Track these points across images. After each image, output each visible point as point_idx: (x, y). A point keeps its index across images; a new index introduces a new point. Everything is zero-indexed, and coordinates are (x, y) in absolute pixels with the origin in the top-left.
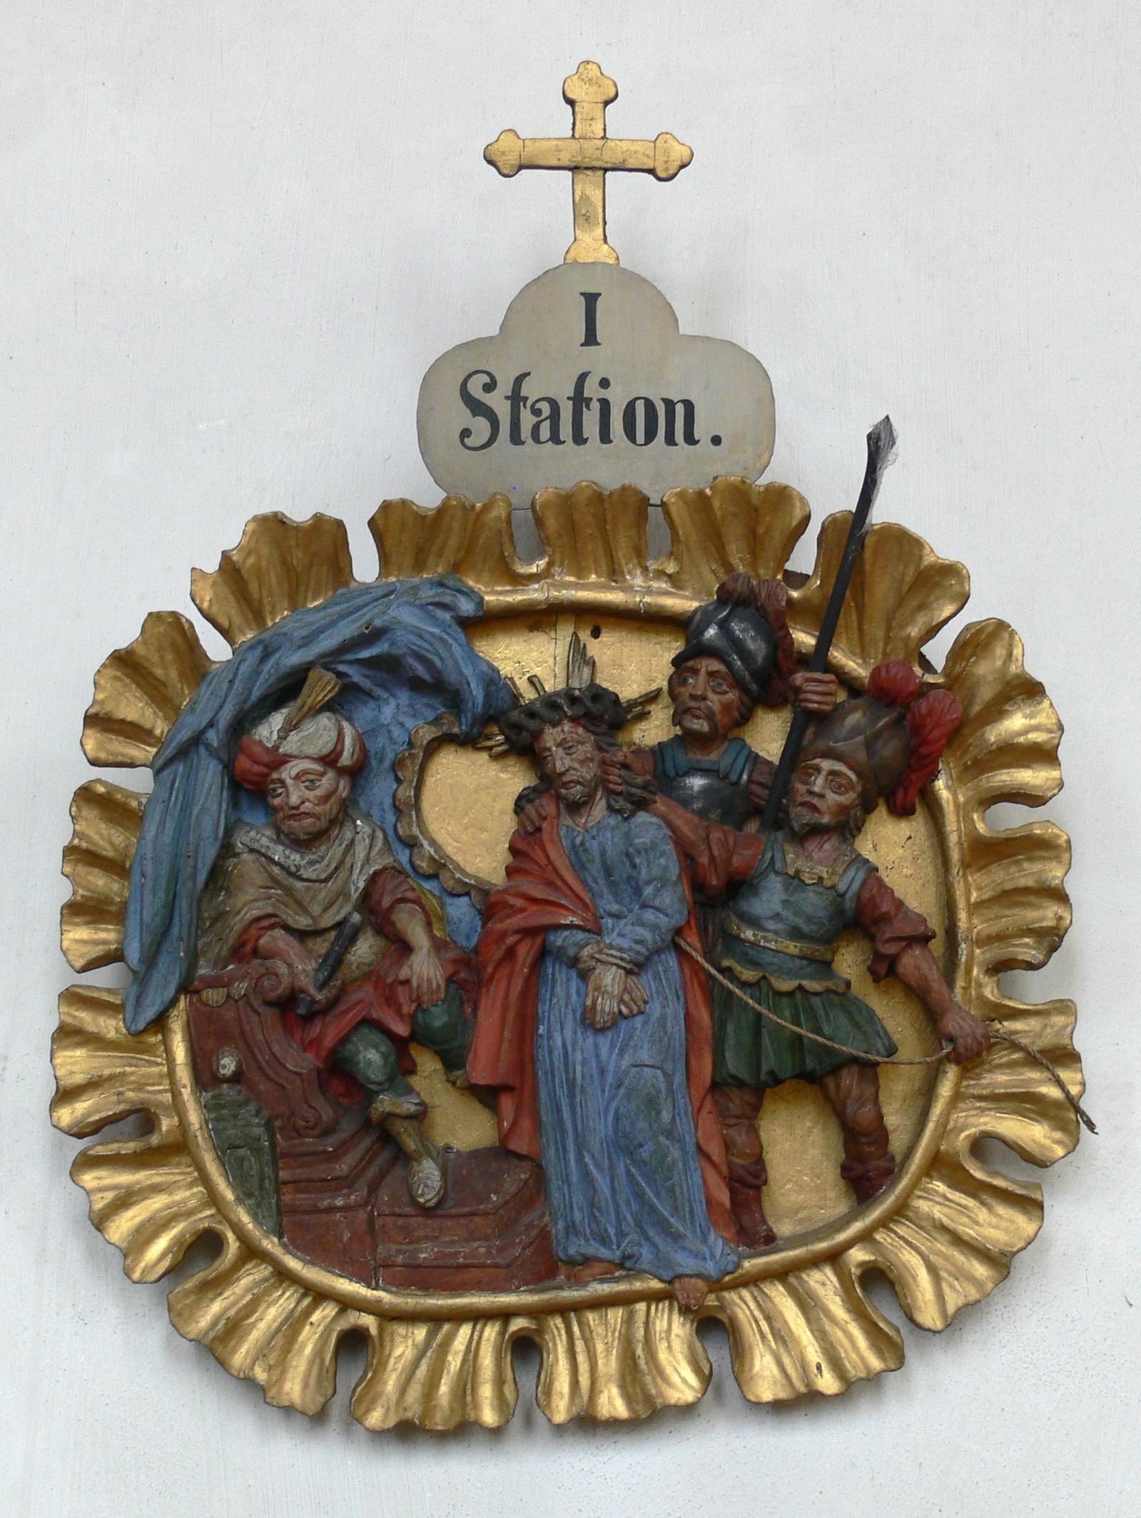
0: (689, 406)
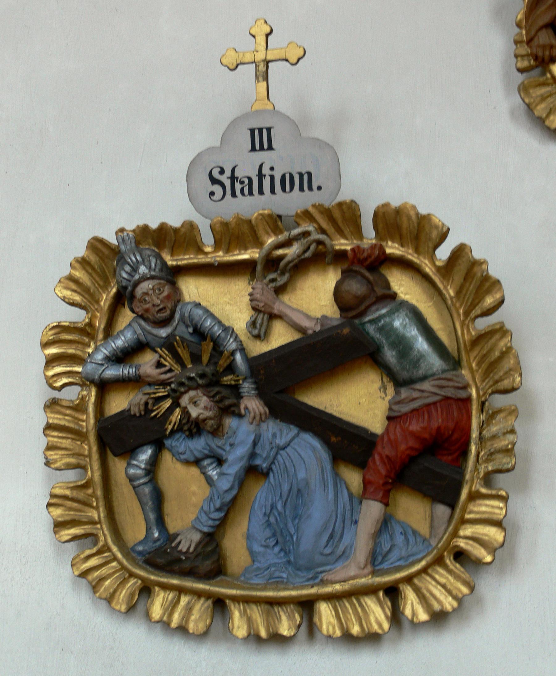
0: (310, 174)
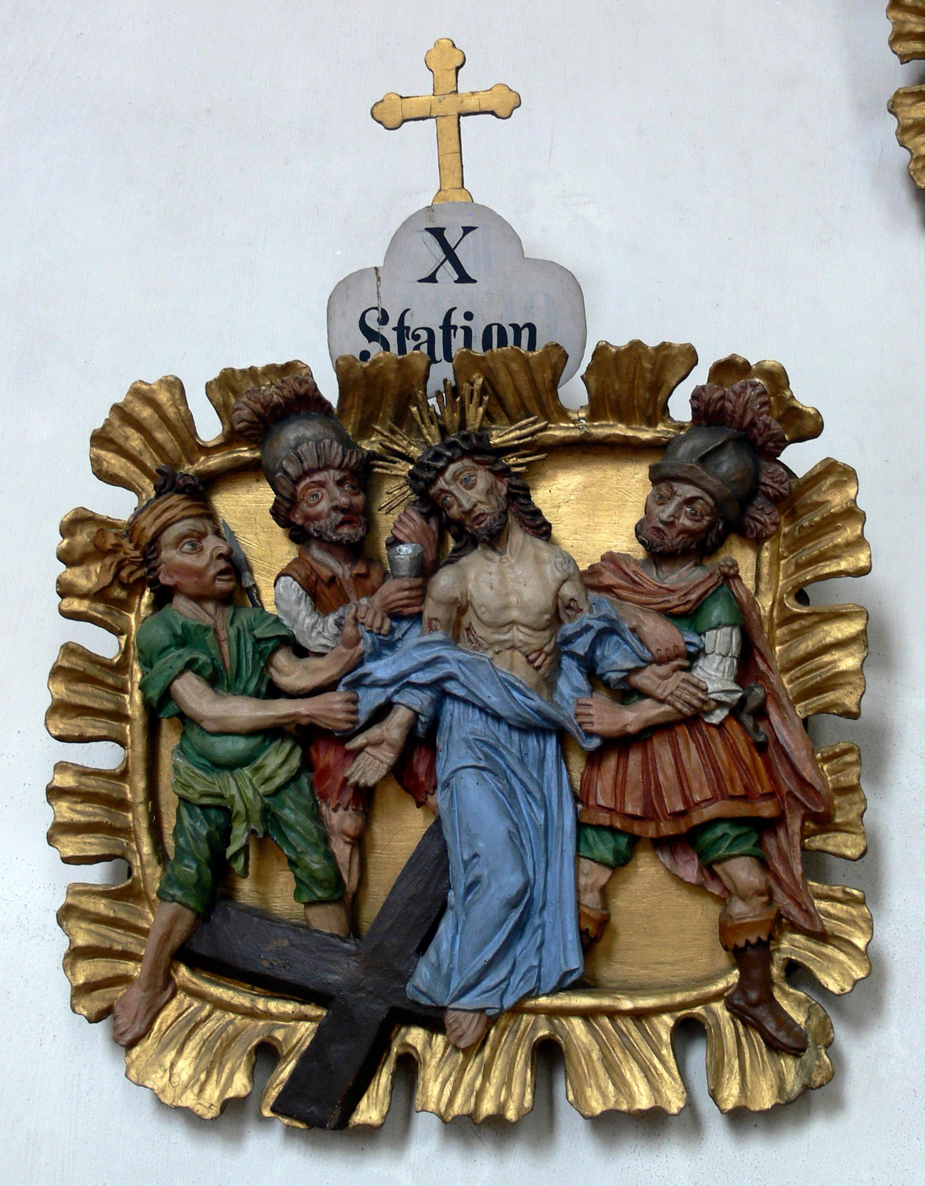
0: (531, 327)
